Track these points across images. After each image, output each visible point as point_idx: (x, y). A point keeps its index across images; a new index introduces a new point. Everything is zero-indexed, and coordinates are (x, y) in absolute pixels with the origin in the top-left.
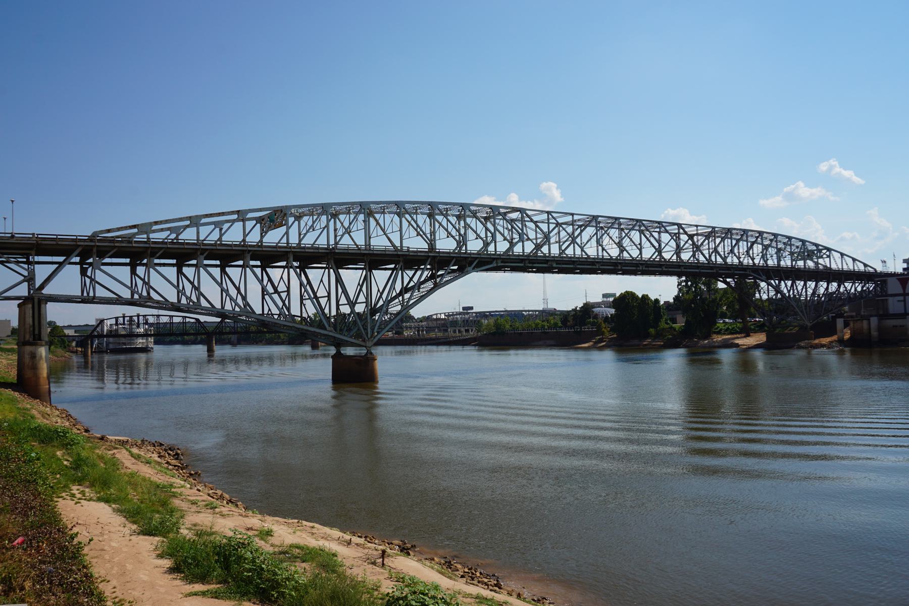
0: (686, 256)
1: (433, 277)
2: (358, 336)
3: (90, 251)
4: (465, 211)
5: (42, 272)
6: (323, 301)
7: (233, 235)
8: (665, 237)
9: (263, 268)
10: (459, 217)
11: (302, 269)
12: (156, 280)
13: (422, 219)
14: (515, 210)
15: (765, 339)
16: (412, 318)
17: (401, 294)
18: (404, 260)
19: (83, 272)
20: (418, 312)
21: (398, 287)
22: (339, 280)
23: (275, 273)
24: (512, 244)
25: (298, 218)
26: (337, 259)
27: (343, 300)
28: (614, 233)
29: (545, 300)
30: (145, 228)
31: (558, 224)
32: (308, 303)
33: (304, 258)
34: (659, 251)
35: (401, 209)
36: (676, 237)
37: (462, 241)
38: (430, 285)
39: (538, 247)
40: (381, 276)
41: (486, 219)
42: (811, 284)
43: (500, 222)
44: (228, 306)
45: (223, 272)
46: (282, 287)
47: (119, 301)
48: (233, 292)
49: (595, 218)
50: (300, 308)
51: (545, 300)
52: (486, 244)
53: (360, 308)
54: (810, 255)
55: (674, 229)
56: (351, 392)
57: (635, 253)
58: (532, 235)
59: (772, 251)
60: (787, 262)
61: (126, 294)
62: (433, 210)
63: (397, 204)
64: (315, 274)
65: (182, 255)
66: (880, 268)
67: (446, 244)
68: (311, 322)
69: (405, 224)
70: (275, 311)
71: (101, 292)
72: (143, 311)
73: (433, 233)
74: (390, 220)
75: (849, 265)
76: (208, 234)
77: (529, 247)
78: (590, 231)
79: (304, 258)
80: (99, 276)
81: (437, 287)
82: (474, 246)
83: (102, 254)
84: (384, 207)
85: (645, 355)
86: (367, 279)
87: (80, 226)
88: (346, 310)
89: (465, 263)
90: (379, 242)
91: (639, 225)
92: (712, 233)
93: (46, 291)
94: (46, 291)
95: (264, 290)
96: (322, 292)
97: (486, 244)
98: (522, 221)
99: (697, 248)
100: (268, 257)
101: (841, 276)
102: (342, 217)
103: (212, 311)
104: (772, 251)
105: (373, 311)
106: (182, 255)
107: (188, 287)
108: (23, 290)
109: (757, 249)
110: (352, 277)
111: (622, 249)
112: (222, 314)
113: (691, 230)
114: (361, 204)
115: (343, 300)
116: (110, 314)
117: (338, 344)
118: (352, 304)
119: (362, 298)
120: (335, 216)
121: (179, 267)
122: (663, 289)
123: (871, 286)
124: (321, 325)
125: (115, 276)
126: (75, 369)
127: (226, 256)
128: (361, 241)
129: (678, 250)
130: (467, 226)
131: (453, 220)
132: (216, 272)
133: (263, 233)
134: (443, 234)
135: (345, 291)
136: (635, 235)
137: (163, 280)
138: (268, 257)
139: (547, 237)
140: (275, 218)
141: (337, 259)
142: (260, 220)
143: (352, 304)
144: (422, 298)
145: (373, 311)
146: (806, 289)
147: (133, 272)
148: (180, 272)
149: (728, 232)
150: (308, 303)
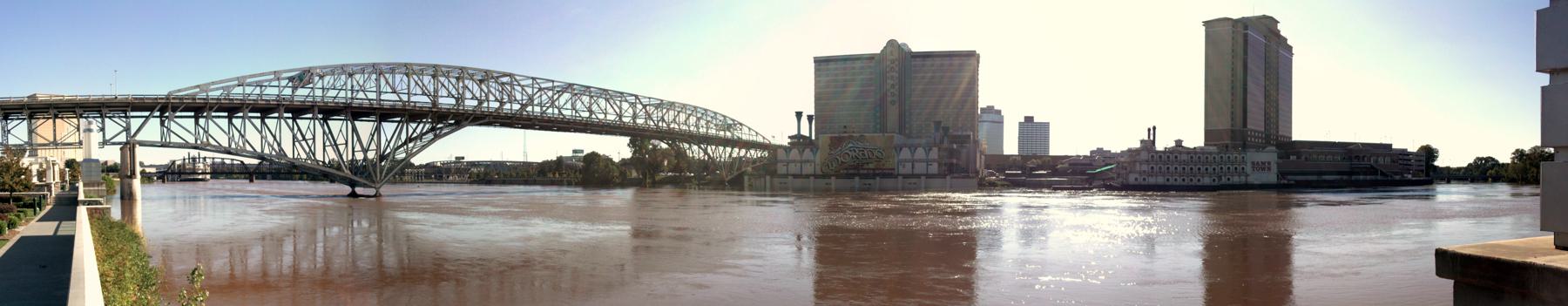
0: (640, 121)
1: (433, 129)
3: (164, 108)
4: (462, 74)
5: (135, 124)
6: (342, 148)
7: (271, 92)
8: (625, 106)
9: (294, 119)
10: (458, 79)
11: (325, 120)
12: (213, 130)
13: (427, 79)
14: (505, 75)
15: (1007, 152)
16: (412, 165)
17: (405, 143)
18: (410, 114)
19: (162, 124)
20: (417, 160)
21: (404, 137)
22: (354, 129)
23: (303, 124)
24: (502, 103)
25: (321, 77)
26: (354, 112)
27: (358, 147)
28: (586, 99)
29: (525, 154)
30: (204, 87)
31: (540, 89)
32: (329, 149)
33: (328, 112)
34: (620, 116)
35: (409, 70)
36: (633, 105)
37: (460, 99)
38: (431, 136)
39: (524, 106)
40: (389, 128)
41: (481, 81)
42: (729, 149)
44: (267, 151)
45: (263, 122)
46: (309, 136)
47: (186, 145)
48: (270, 139)
49: (571, 85)
50: (325, 155)
51: (525, 154)
52: (481, 102)
53: (371, 155)
54: (729, 127)
57: (601, 116)
58: (519, 97)
59: (703, 122)
60: (713, 132)
61: (191, 140)
62: (436, 72)
63: (406, 65)
64: (336, 125)
65: (232, 109)
66: (773, 142)
67: (446, 102)
68: (331, 165)
69: (413, 84)
70: (304, 156)
71: (174, 139)
72: (203, 154)
73: (436, 91)
74: (400, 81)
75: (760, 139)
76: (252, 92)
77: (516, 107)
78: (566, 96)
79: (328, 112)
80: (174, 127)
81: (437, 137)
82: (470, 104)
83: (175, 109)
84: (393, 69)
85: (1167, 204)
86: (378, 130)
87: (157, 88)
88: (360, 156)
89: (461, 118)
90: (389, 98)
91: (606, 94)
92: (660, 105)
93: (139, 138)
94: (139, 138)
95: (294, 137)
96: (341, 140)
97: (481, 102)
98: (511, 84)
99: (649, 116)
100: (297, 111)
102: (357, 76)
103: (254, 155)
104: (703, 122)
105: (382, 157)
106: (232, 109)
107: (237, 134)
108: (123, 138)
109: (692, 120)
110: (365, 127)
112: (261, 157)
113: (645, 101)
114: (374, 65)
115: (358, 147)
116: (178, 155)
117: (353, 184)
118: (365, 151)
119: (373, 146)
120: (351, 75)
121: (230, 118)
122: (617, 149)
123: (766, 154)
124: (339, 168)
125: (184, 127)
126: (826, 221)
127: (265, 110)
128: (372, 96)
129: (635, 116)
130: (465, 87)
131: (453, 81)
132: (258, 122)
133: (295, 88)
134: (444, 93)
135: (359, 140)
136: (602, 102)
137: (218, 129)
138: (297, 111)
139: (531, 99)
140: (302, 78)
141: (354, 112)
142: (291, 79)
143: (365, 151)
144: (424, 147)
145: (382, 157)
146: (722, 154)
147: (197, 123)
148: (230, 122)
149: (672, 105)
150: (329, 149)
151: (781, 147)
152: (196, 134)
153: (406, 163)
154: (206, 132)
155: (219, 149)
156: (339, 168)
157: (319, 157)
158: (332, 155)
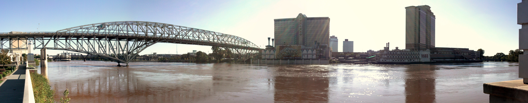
0: (215, 41)
1: (146, 44)
2: (124, 60)
3: (55, 36)
4: (156, 25)
5: (45, 42)
6: (115, 50)
8: (211, 36)
9: (99, 40)
10: (154, 27)
11: (110, 40)
12: (72, 44)
13: (144, 27)
14: (170, 25)
15: (339, 51)
16: (139, 56)
17: (136, 48)
18: (138, 38)
19: (55, 42)
20: (140, 54)
21: (136, 46)
22: (119, 44)
23: (102, 42)
24: (169, 35)
25: (108, 26)
26: (119, 38)
27: (120, 50)
28: (197, 33)
29: (177, 52)
31: (182, 30)
32: (111, 50)
33: (110, 38)
35: (138, 24)
36: (213, 35)
37: (155, 33)
38: (145, 46)
39: (176, 36)
40: (131, 43)
41: (162, 27)
42: (245, 50)
43: (166, 28)
44: (90, 51)
45: (89, 41)
46: (104, 46)
47: (63, 49)
48: (91, 47)
49: (192, 29)
50: (109, 52)
51: (177, 52)
52: (162, 34)
53: (125, 52)
54: (245, 43)
55: (213, 33)
56: (473, 66)
57: (202, 39)
58: (175, 33)
59: (237, 41)
60: (240, 44)
61: (64, 47)
62: (147, 24)
63: (137, 22)
64: (113, 42)
65: (78, 37)
66: (260, 48)
67: (150, 34)
68: (111, 55)
69: (139, 28)
70: (102, 52)
71: (59, 47)
72: (69, 52)
73: (147, 31)
74: (135, 27)
75: (256, 47)
76: (85, 31)
77: (174, 36)
78: (191, 32)
79: (110, 38)
80: (58, 43)
81: (147, 46)
82: (158, 35)
83: (59, 37)
84: (132, 23)
86: (127, 44)
88: (121, 53)
89: (155, 40)
90: (131, 33)
92: (222, 35)
95: (99, 46)
96: (115, 47)
97: (162, 34)
99: (218, 39)
100: (100, 37)
101: (252, 49)
102: (120, 26)
103: (86, 52)
104: (237, 41)
105: (129, 53)
106: (78, 37)
107: (80, 45)
108: (41, 46)
109: (233, 40)
110: (123, 43)
111: (199, 38)
112: (88, 53)
113: (217, 34)
114: (126, 22)
115: (120, 50)
116: (60, 52)
117: (119, 62)
118: (123, 51)
119: (126, 49)
120: (118, 25)
121: (77, 40)
122: (208, 50)
123: (258, 52)
124: (114, 57)
125: (62, 43)
127: (89, 37)
129: (214, 39)
131: (153, 27)
132: (87, 41)
133: (99, 30)
134: (150, 31)
135: (121, 47)
136: (203, 34)
137: (73, 43)
138: (100, 37)
139: (179, 33)
140: (102, 26)
142: (98, 27)
143: (123, 51)
144: (143, 50)
145: (129, 53)
146: (243, 52)
147: (66, 41)
148: (78, 41)
149: (226, 35)
150: (111, 50)
151: (263, 49)
152: (66, 45)
153: (137, 55)
154: (69, 44)
155: (74, 50)
156: (114, 57)
157: (108, 53)
158: (112, 52)
